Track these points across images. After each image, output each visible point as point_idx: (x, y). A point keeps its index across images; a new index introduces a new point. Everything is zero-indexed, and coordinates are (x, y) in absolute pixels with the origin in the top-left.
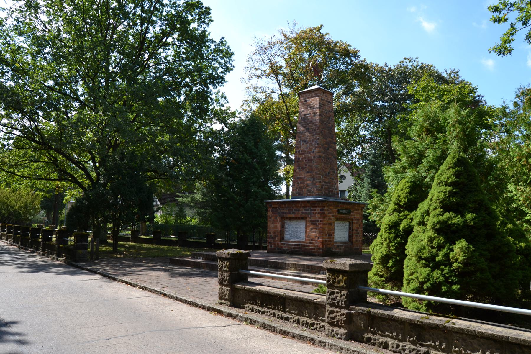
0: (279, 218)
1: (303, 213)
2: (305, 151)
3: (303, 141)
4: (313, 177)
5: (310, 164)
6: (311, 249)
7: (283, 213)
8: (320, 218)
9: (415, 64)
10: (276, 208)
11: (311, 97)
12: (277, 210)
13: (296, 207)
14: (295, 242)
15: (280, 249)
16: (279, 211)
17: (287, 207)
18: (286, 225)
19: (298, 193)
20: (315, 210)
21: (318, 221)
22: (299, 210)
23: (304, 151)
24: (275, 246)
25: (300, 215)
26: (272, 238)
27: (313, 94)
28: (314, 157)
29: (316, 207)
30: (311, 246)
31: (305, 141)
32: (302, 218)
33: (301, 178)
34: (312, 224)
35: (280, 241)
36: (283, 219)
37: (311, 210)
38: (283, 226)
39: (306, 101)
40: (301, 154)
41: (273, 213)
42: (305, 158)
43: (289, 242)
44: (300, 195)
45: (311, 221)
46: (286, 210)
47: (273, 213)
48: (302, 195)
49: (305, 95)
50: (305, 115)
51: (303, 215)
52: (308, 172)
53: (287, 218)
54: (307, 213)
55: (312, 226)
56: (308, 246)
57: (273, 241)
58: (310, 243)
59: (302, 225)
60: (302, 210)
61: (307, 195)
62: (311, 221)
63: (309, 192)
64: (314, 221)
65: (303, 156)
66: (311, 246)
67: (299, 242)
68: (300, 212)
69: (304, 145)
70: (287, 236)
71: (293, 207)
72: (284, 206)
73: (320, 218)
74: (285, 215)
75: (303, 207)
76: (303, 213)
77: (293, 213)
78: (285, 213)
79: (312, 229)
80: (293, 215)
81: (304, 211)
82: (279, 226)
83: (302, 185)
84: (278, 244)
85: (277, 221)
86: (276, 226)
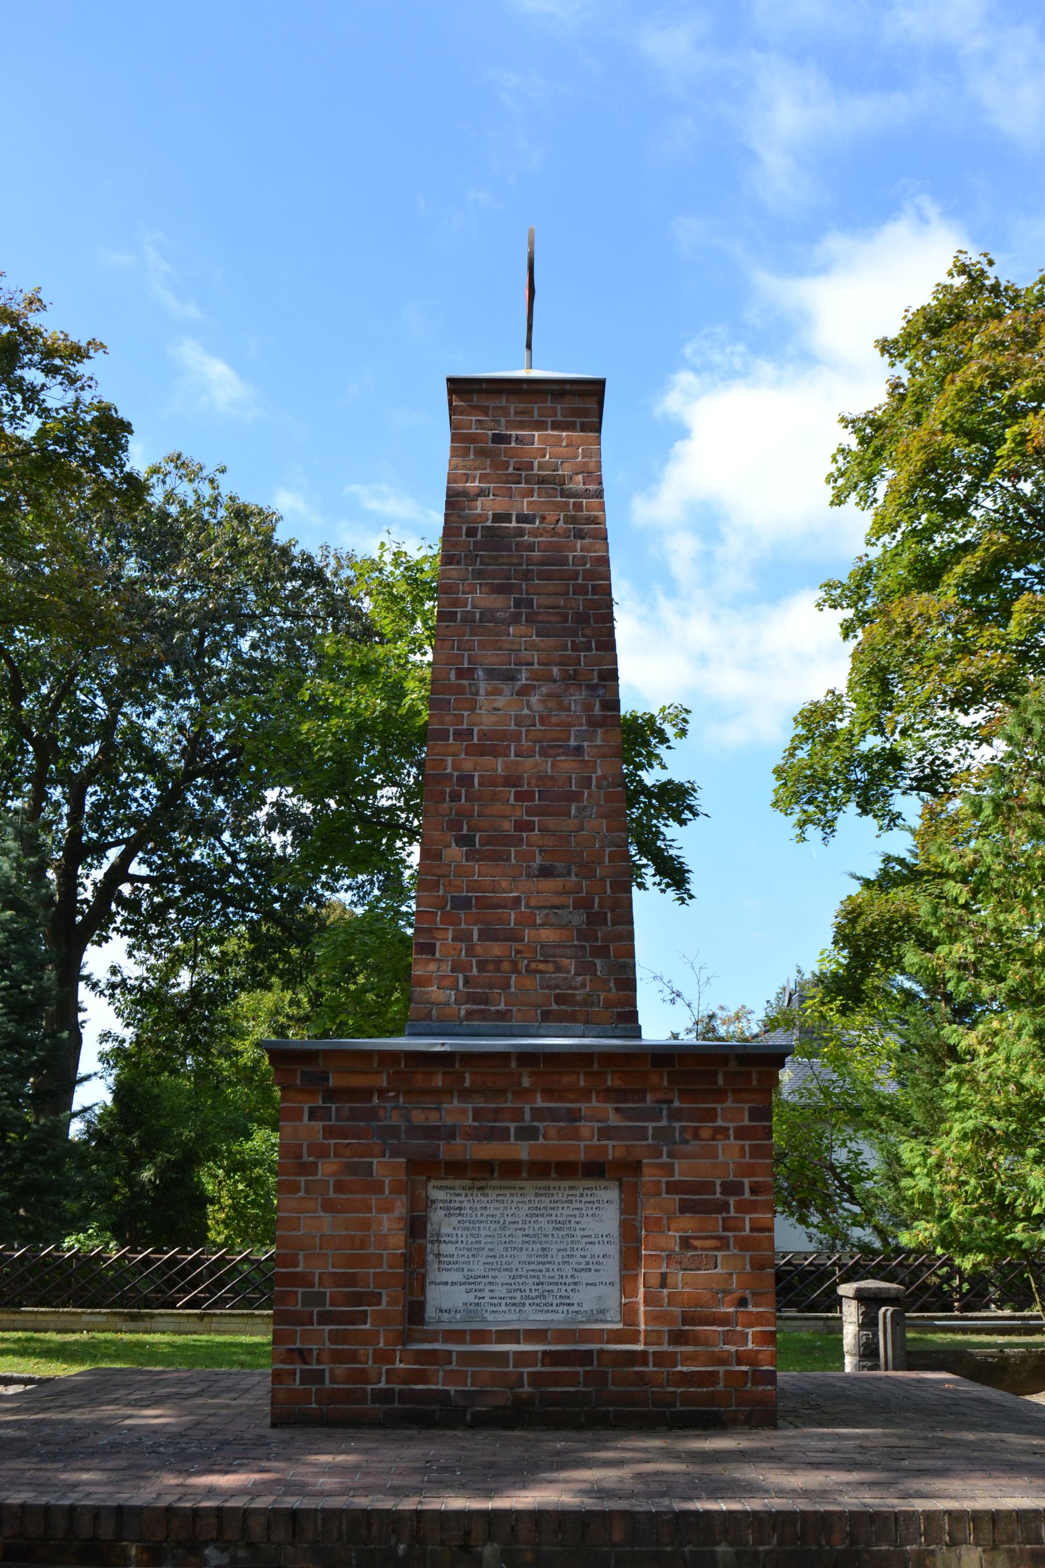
0: (386, 1169)
1: (606, 1133)
2: (516, 737)
3: (491, 674)
4: (583, 904)
5: (551, 822)
6: (687, 1378)
7: (432, 1132)
8: (749, 1170)
9: (207, 491)
10: (365, 1093)
11: (540, 426)
12: (372, 1114)
13: (549, 1093)
14: (534, 1335)
15: (406, 1397)
16: (395, 1119)
17: (465, 1094)
18: (437, 1216)
19: (471, 998)
20: (711, 1115)
21: (732, 1188)
22: (574, 1116)
23: (503, 735)
24: (362, 1376)
25: (585, 1143)
26: (326, 1318)
27: (559, 410)
28: (586, 782)
29: (720, 1095)
30: (687, 1358)
31: (510, 677)
32: (595, 1170)
33: (484, 904)
34: (685, 1208)
35: (405, 1338)
36: (430, 1166)
37: (675, 1115)
38: (417, 1227)
39: (498, 439)
40: (481, 751)
41: (329, 1132)
42: (511, 781)
43: (480, 1336)
44: (484, 1015)
45: (673, 1188)
46: (457, 1112)
47: (329, 1132)
48: (502, 1016)
49: (491, 403)
50: (497, 518)
51: (614, 1150)
52: (546, 872)
53: (456, 1169)
54: (641, 1133)
55: (688, 1223)
56: (660, 1358)
57: (335, 1337)
58: (678, 1337)
59: (596, 1217)
60: (599, 1112)
61: (546, 1016)
62: (673, 1188)
63: (560, 999)
64: (706, 1187)
65: (499, 765)
66: (687, 1358)
67: (563, 1335)
68: (586, 1127)
69: (501, 701)
70: (447, 1297)
71: (522, 1094)
72: (439, 1081)
73: (749, 1170)
74: (446, 1150)
75: (610, 1094)
76: (606, 1133)
77: (527, 1134)
78: (451, 1133)
79: (686, 1243)
80: (523, 1151)
81: (614, 1121)
82: (389, 1226)
83: (497, 949)
84: (383, 1357)
85: (377, 1187)
86: (365, 1225)
